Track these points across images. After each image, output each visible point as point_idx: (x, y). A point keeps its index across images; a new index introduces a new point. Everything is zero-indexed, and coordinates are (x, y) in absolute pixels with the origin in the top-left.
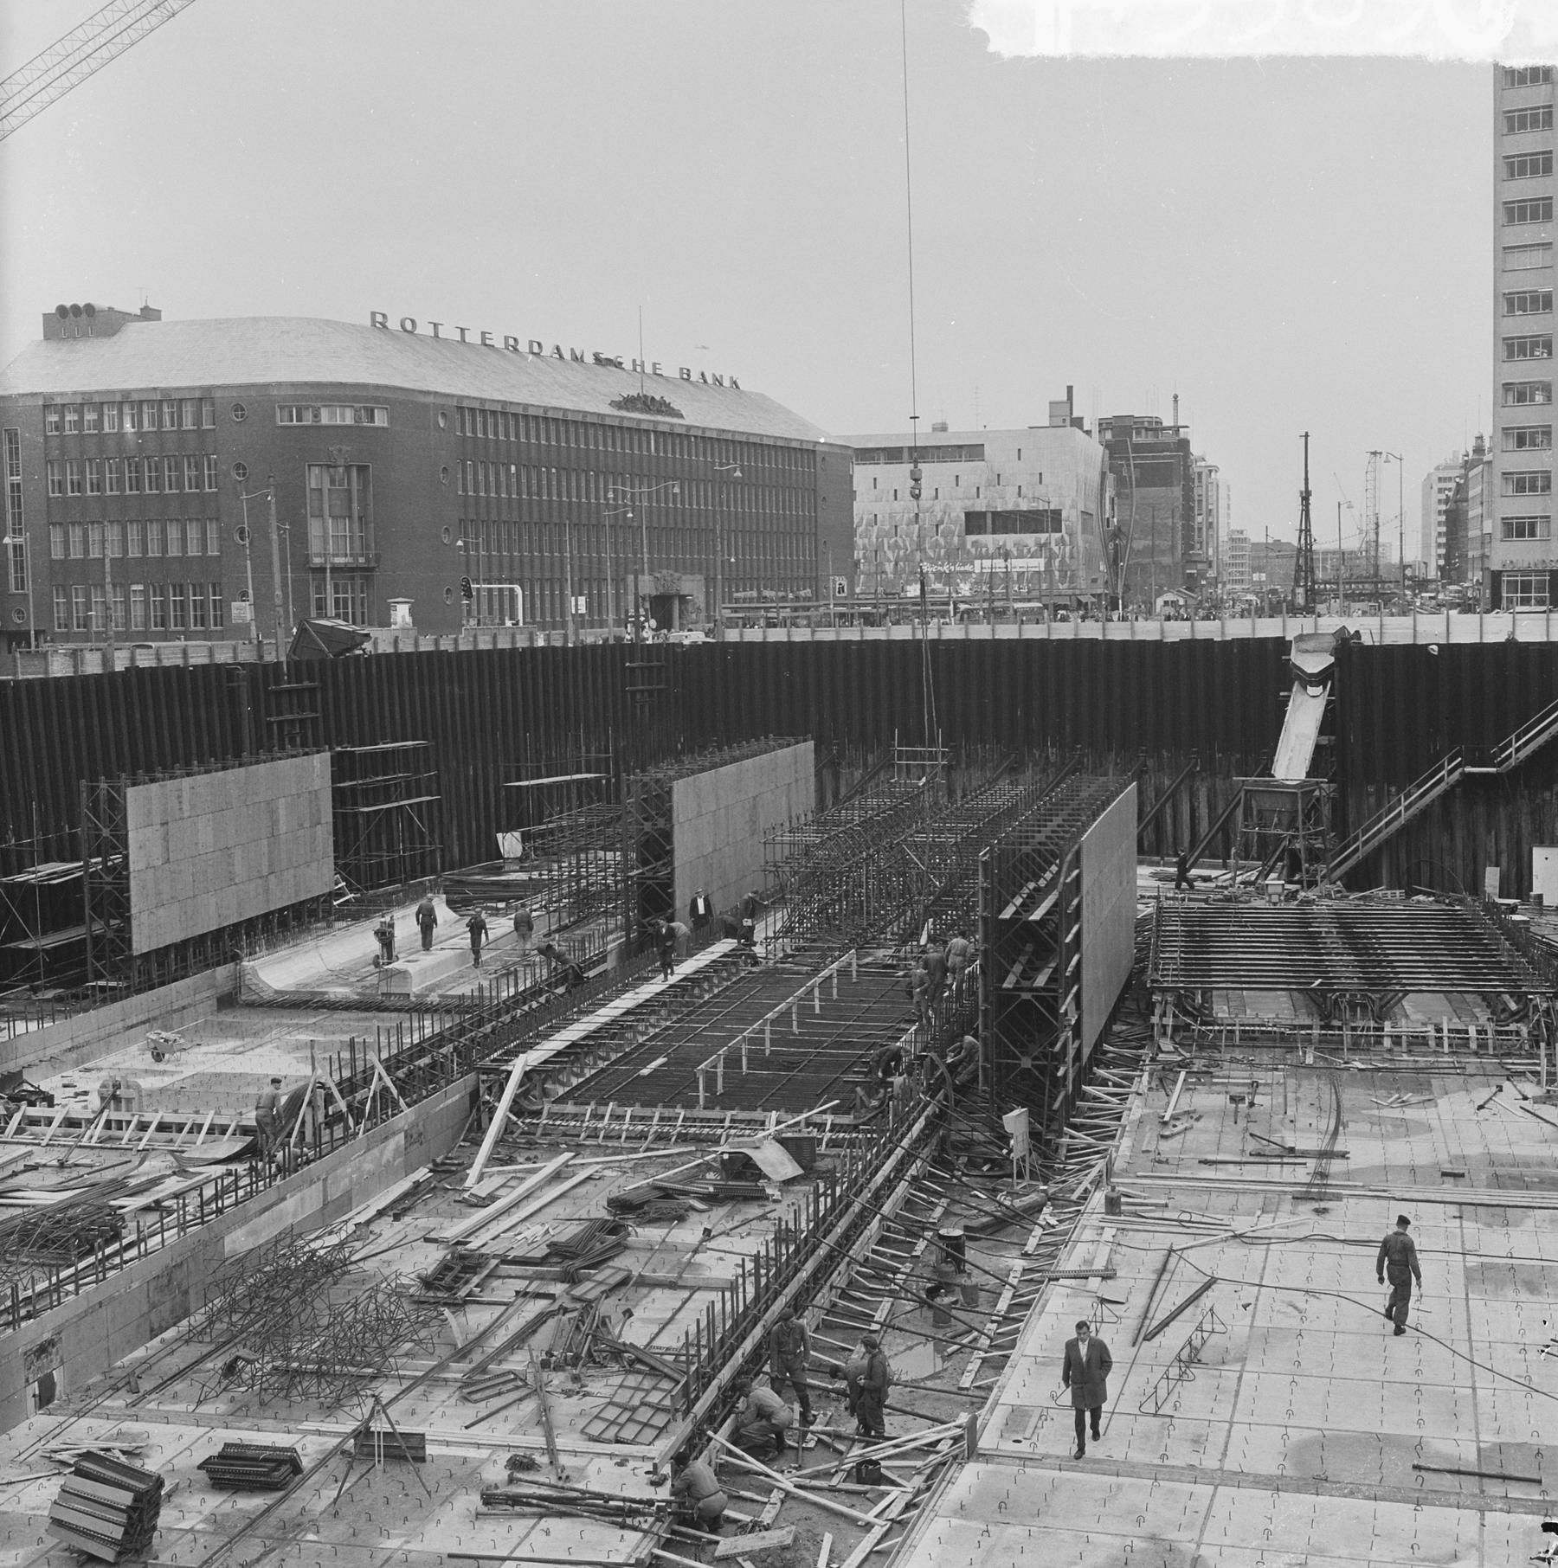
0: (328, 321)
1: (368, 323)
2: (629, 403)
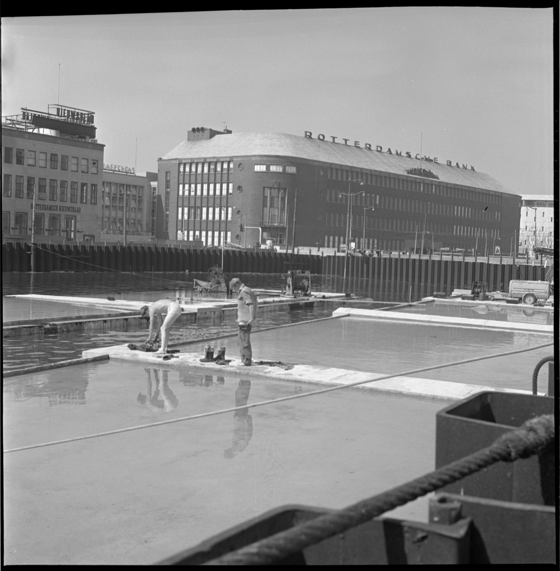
0: (291, 135)
1: (304, 135)
2: (410, 172)
